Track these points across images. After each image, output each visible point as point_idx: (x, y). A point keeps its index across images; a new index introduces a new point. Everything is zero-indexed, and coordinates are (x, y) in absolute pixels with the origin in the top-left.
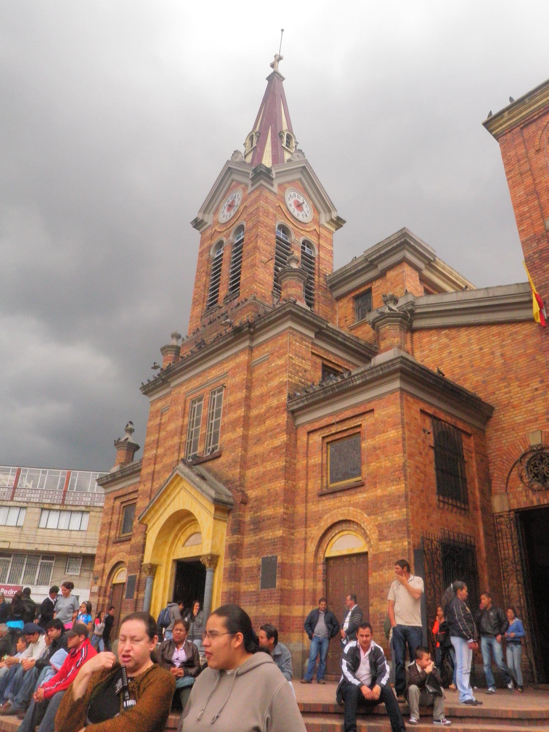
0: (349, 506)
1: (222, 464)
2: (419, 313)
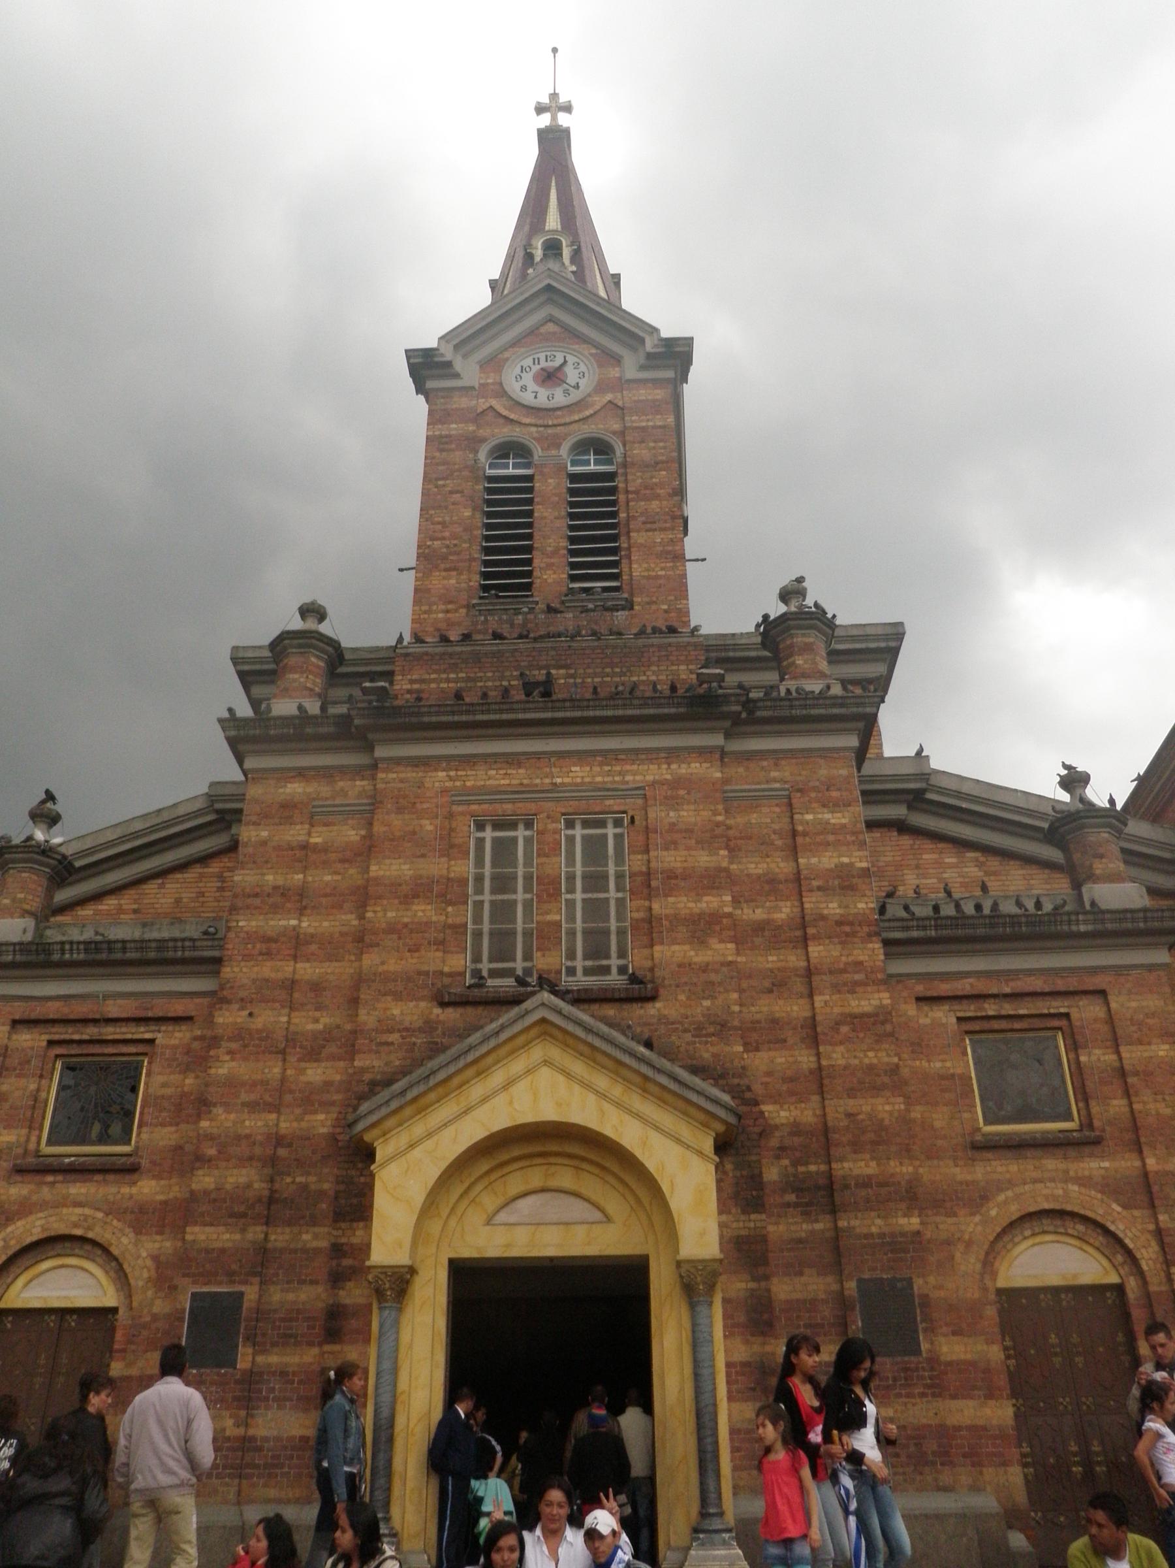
0: (1066, 1182)
1: (663, 1019)
2: (932, 802)
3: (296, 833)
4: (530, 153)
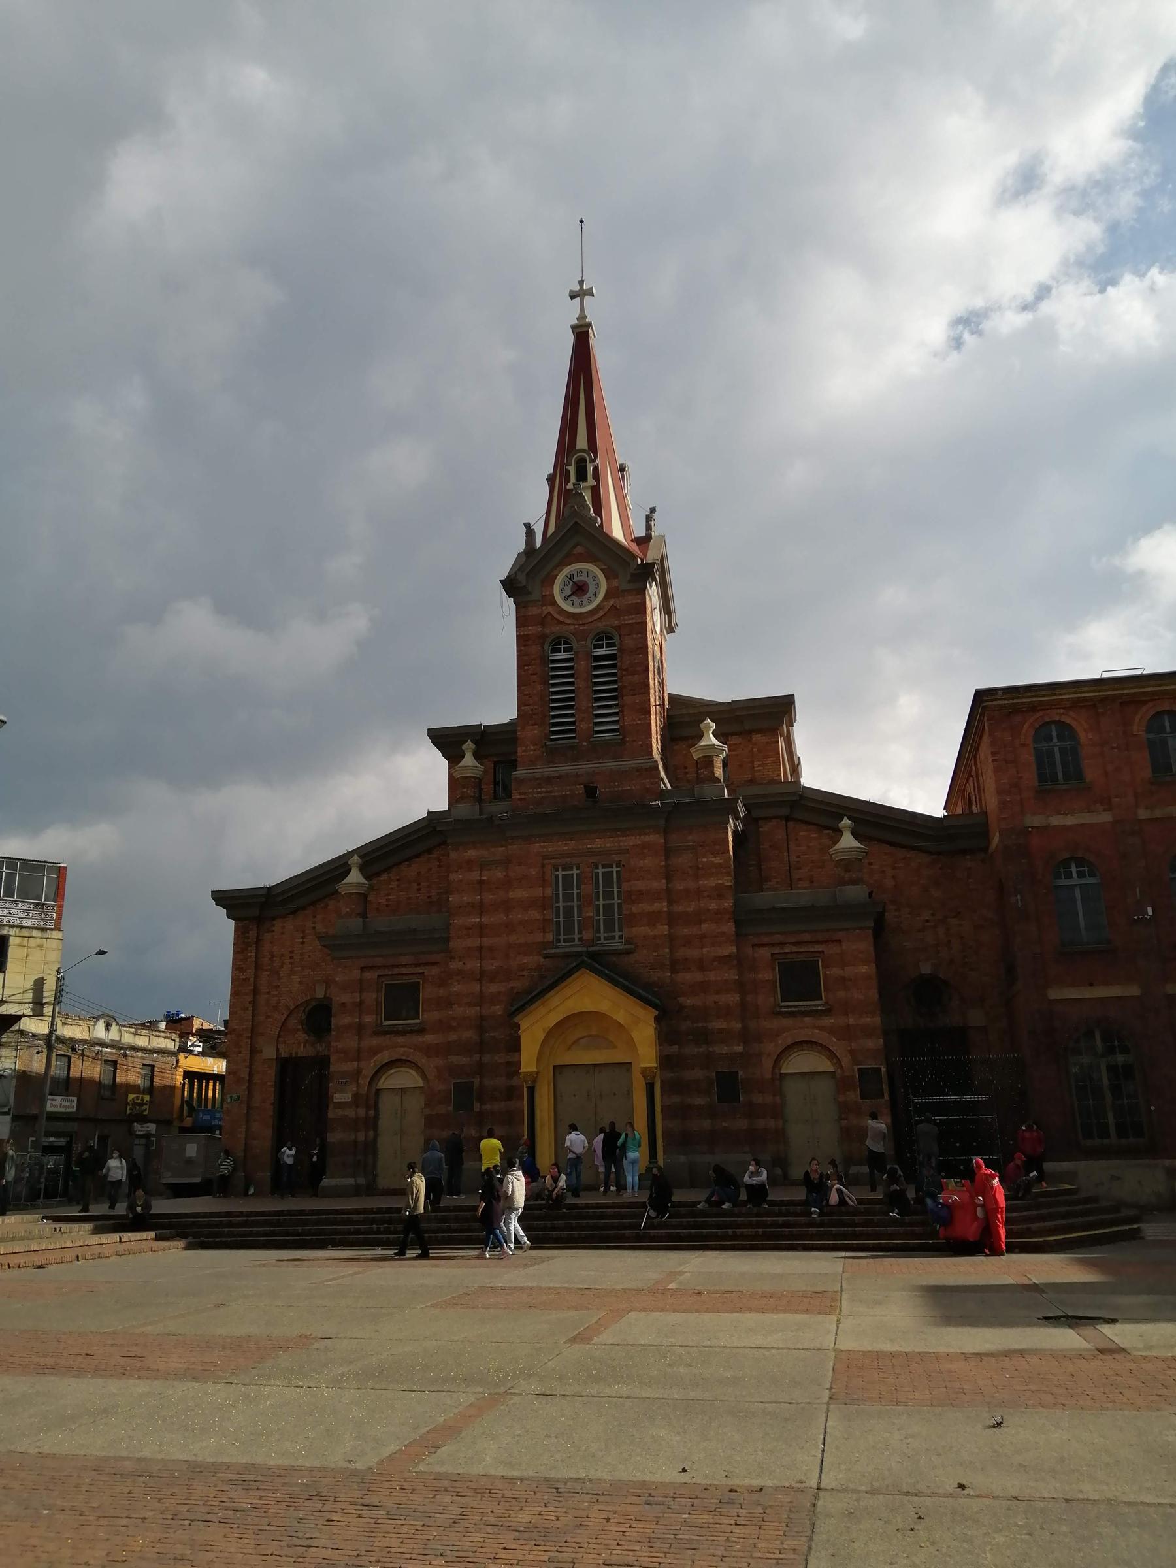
3: (475, 875)
4: (570, 339)
